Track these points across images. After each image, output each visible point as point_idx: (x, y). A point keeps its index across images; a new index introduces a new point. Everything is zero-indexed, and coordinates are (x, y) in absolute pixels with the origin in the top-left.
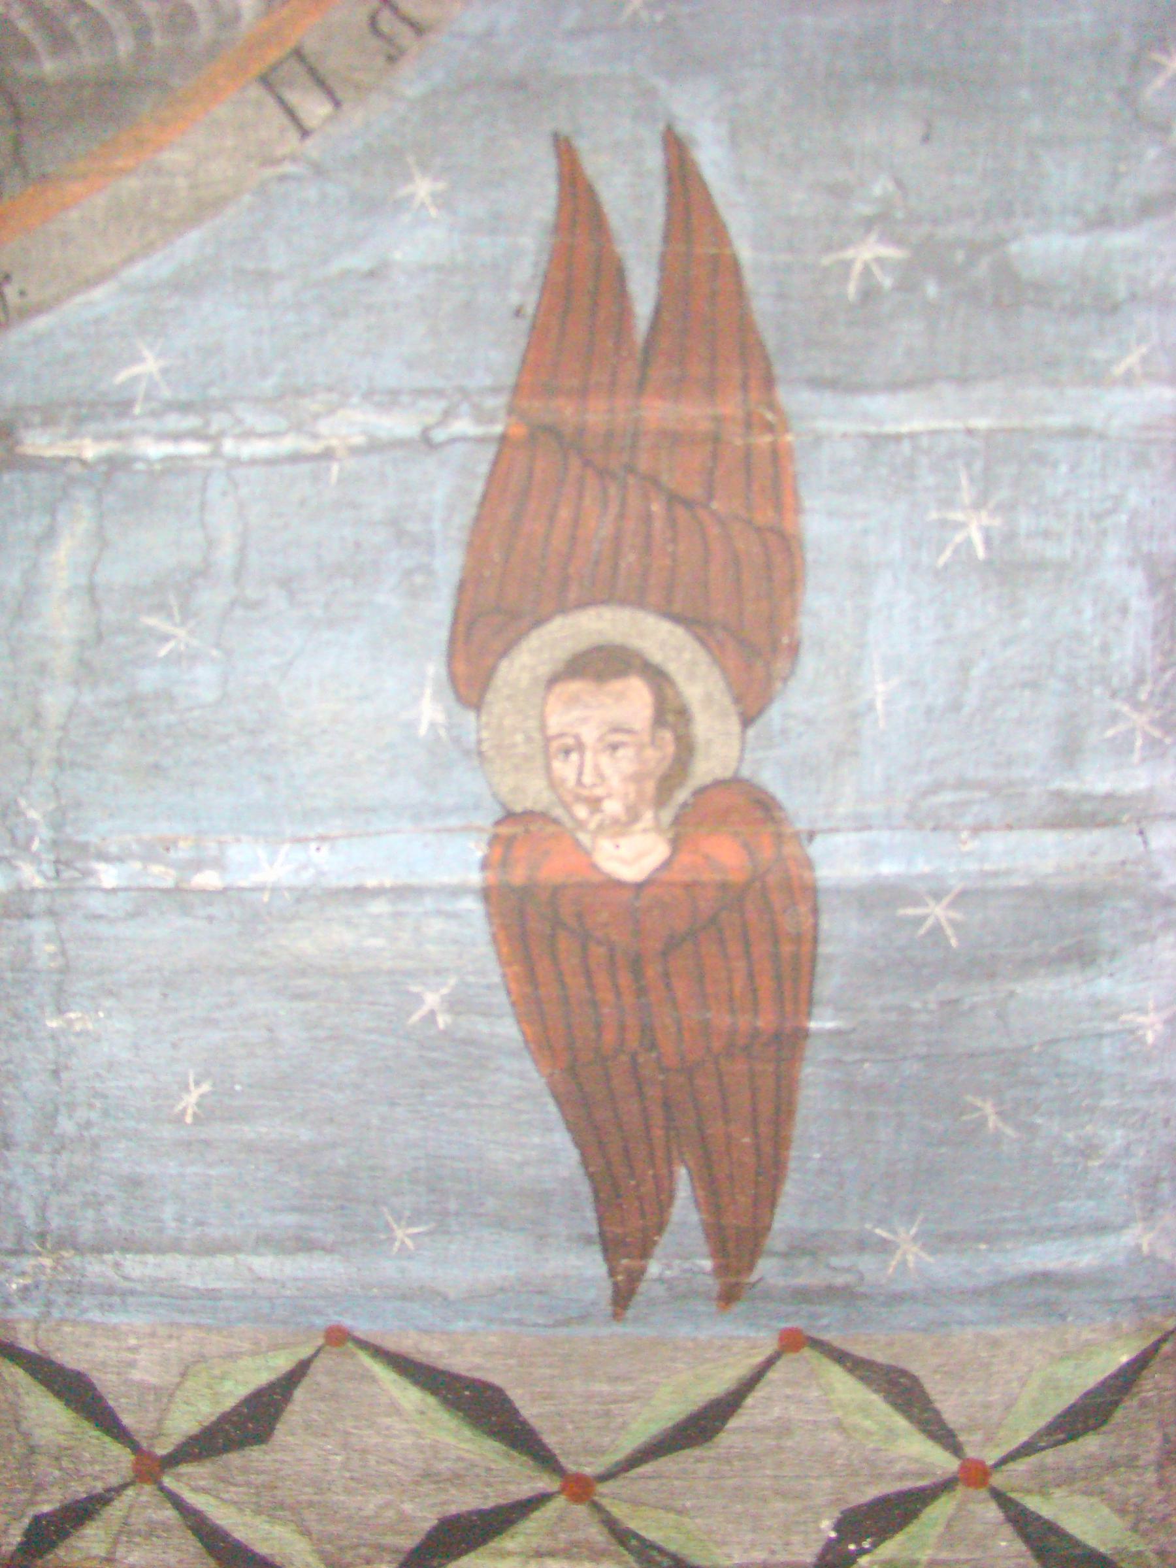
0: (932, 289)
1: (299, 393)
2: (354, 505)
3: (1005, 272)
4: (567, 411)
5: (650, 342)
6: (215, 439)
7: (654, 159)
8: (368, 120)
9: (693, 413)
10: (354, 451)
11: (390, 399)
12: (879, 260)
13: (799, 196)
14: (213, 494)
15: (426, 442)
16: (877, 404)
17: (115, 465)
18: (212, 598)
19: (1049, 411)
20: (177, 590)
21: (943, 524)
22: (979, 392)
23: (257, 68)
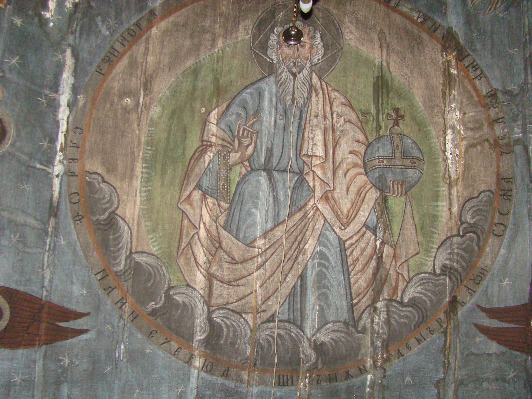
0: (60, 371)
1: (54, 266)
2: (34, 273)
3: (61, 383)
4: (45, 310)
5: (56, 325)
6: (48, 252)
7: (85, 328)
8: (96, 284)
9: (42, 331)
10: (43, 275)
11: (51, 281)
12: (65, 362)
13: (77, 350)
14: (39, 250)
15: (43, 287)
16: (41, 362)
17: (47, 233)
18: (21, 246)
19: (37, 391)
20: (23, 240)
21: (19, 373)
22: (42, 379)
23: (106, 268)
